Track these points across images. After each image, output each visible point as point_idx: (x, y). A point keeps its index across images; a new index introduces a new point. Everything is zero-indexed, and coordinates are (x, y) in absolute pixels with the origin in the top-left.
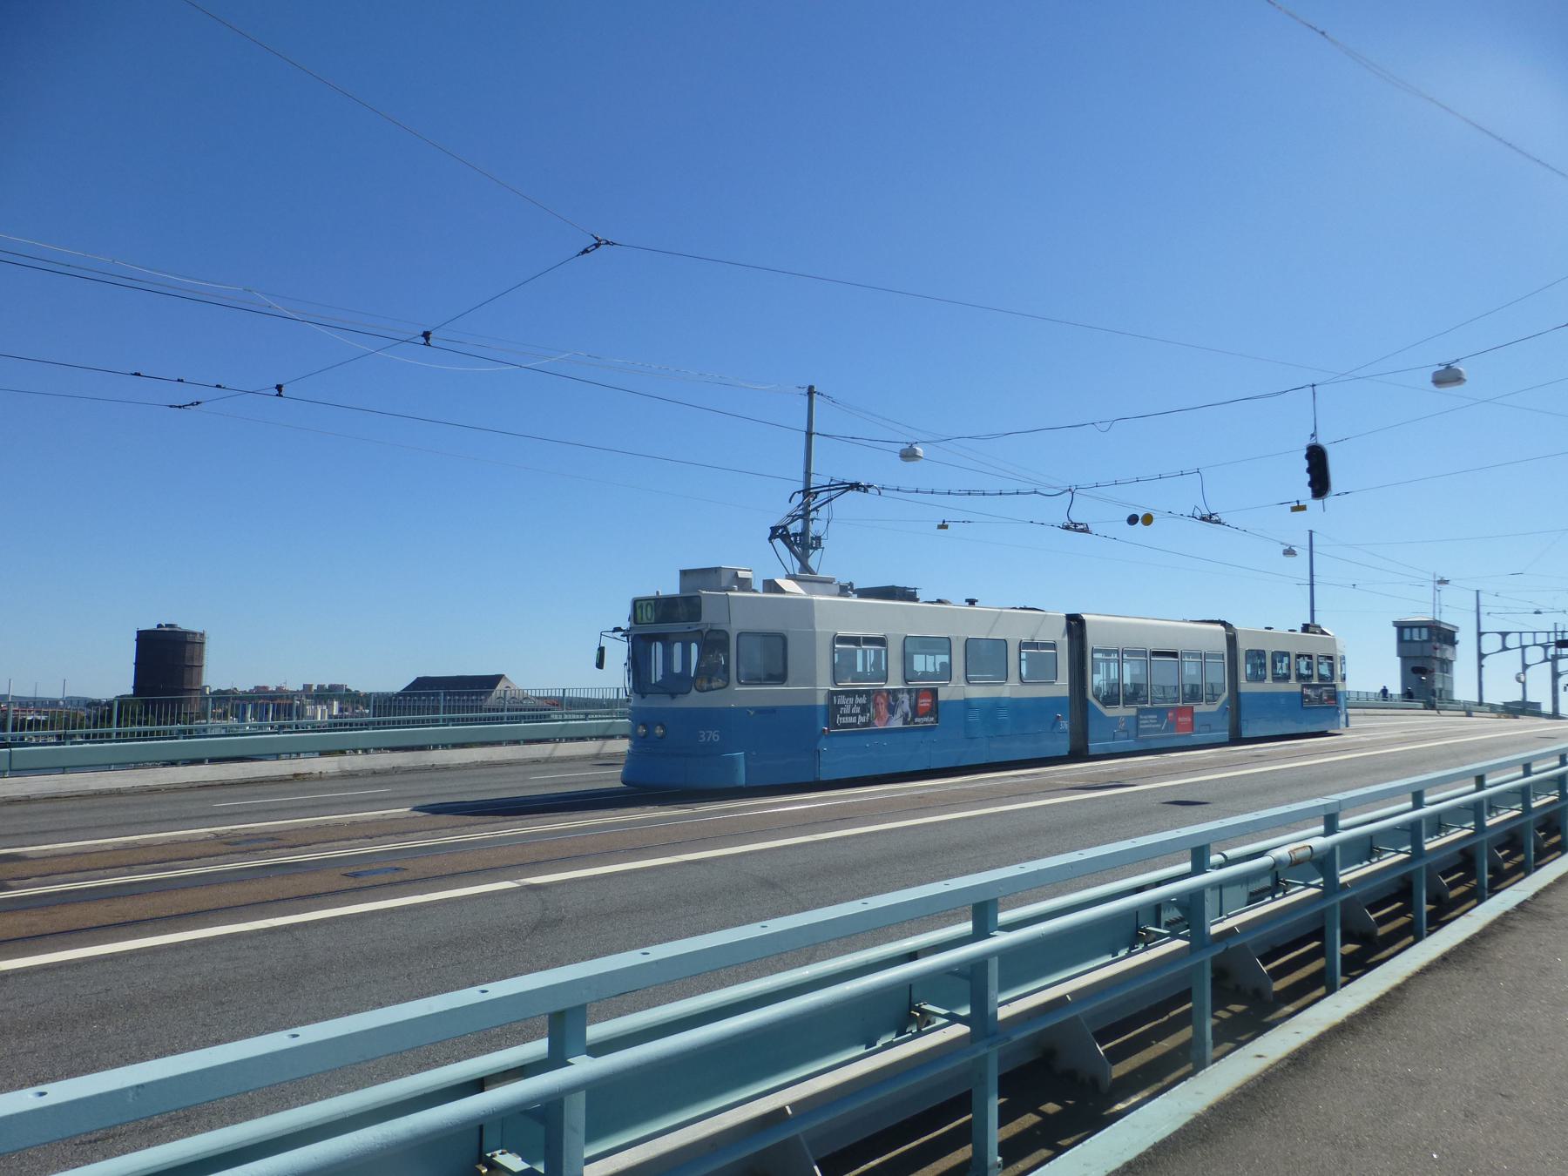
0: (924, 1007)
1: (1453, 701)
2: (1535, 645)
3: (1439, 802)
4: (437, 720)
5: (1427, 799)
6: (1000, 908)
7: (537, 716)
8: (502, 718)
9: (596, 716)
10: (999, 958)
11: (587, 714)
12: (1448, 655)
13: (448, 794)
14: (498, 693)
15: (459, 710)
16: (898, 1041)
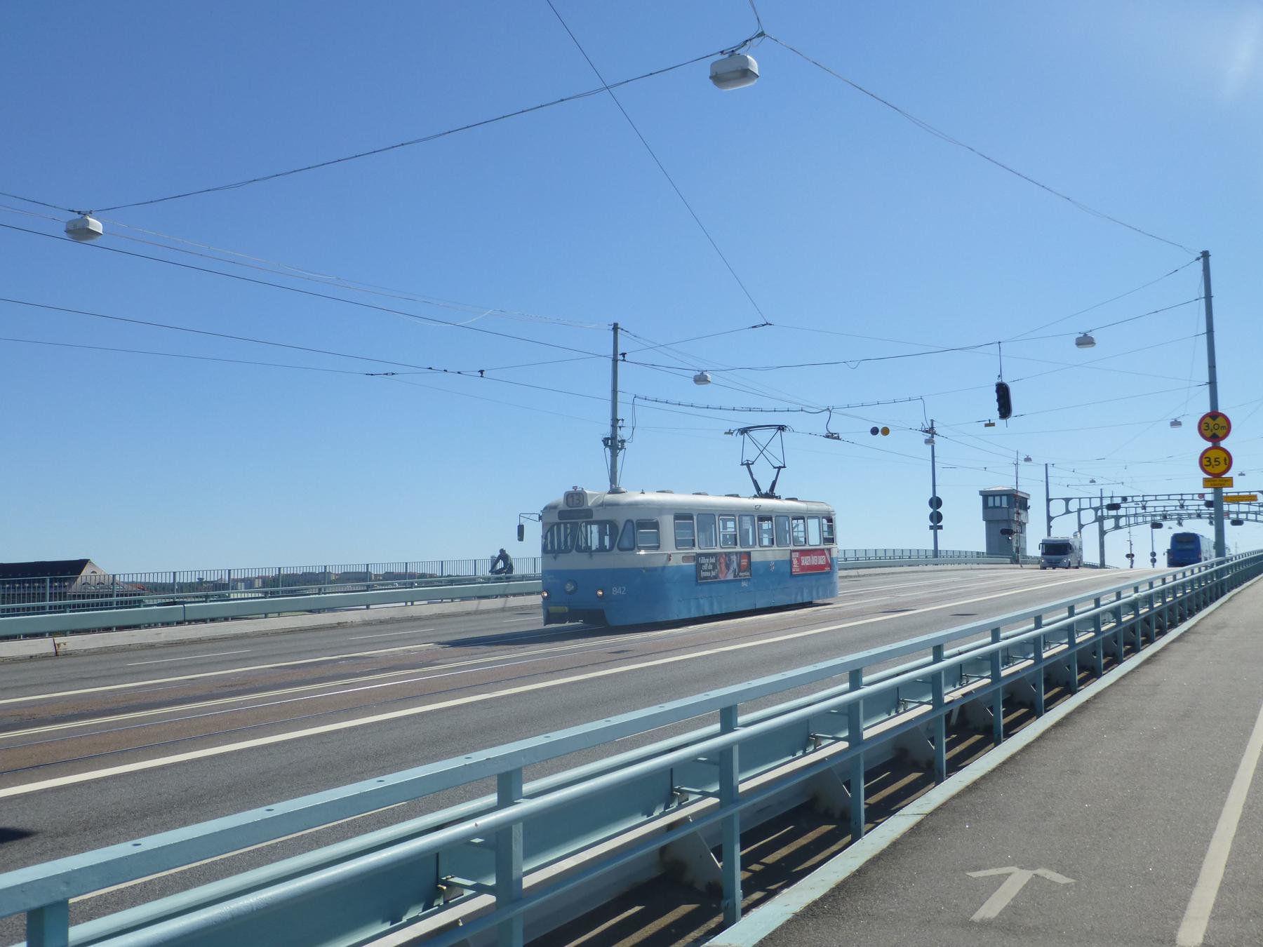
0: (452, 880)
1: (1026, 557)
2: (1091, 508)
3: (898, 675)
4: (43, 608)
5: (1044, 622)
6: (1001, 631)
7: (127, 602)
8: (111, 603)
9: (197, 600)
10: (739, 746)
11: (207, 597)
12: (1022, 518)
13: (495, 629)
14: (84, 578)
15: (56, 597)
16: (424, 915)
